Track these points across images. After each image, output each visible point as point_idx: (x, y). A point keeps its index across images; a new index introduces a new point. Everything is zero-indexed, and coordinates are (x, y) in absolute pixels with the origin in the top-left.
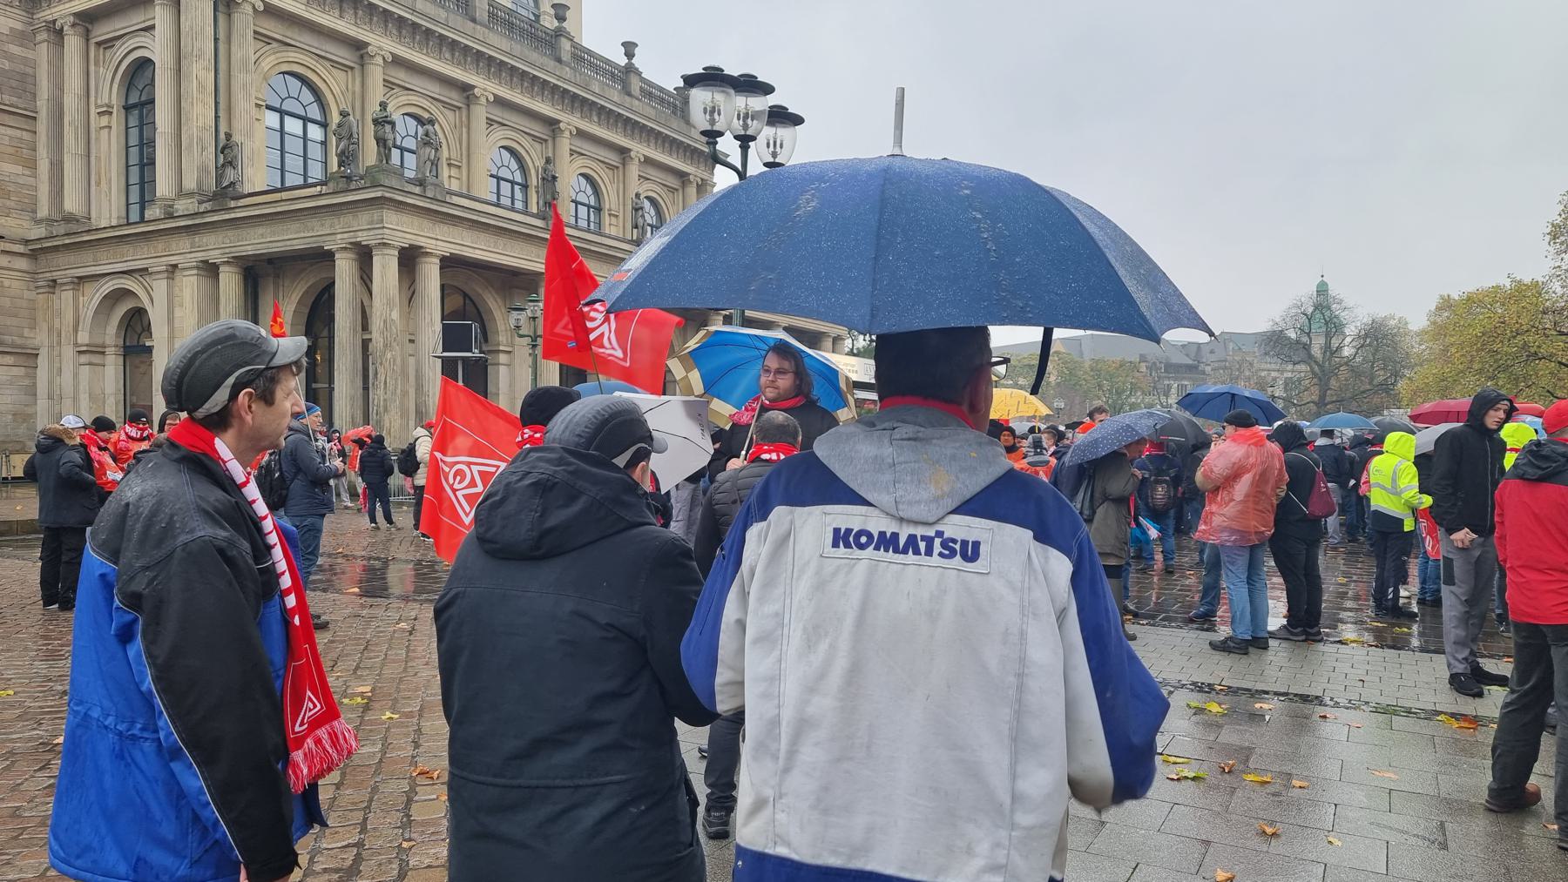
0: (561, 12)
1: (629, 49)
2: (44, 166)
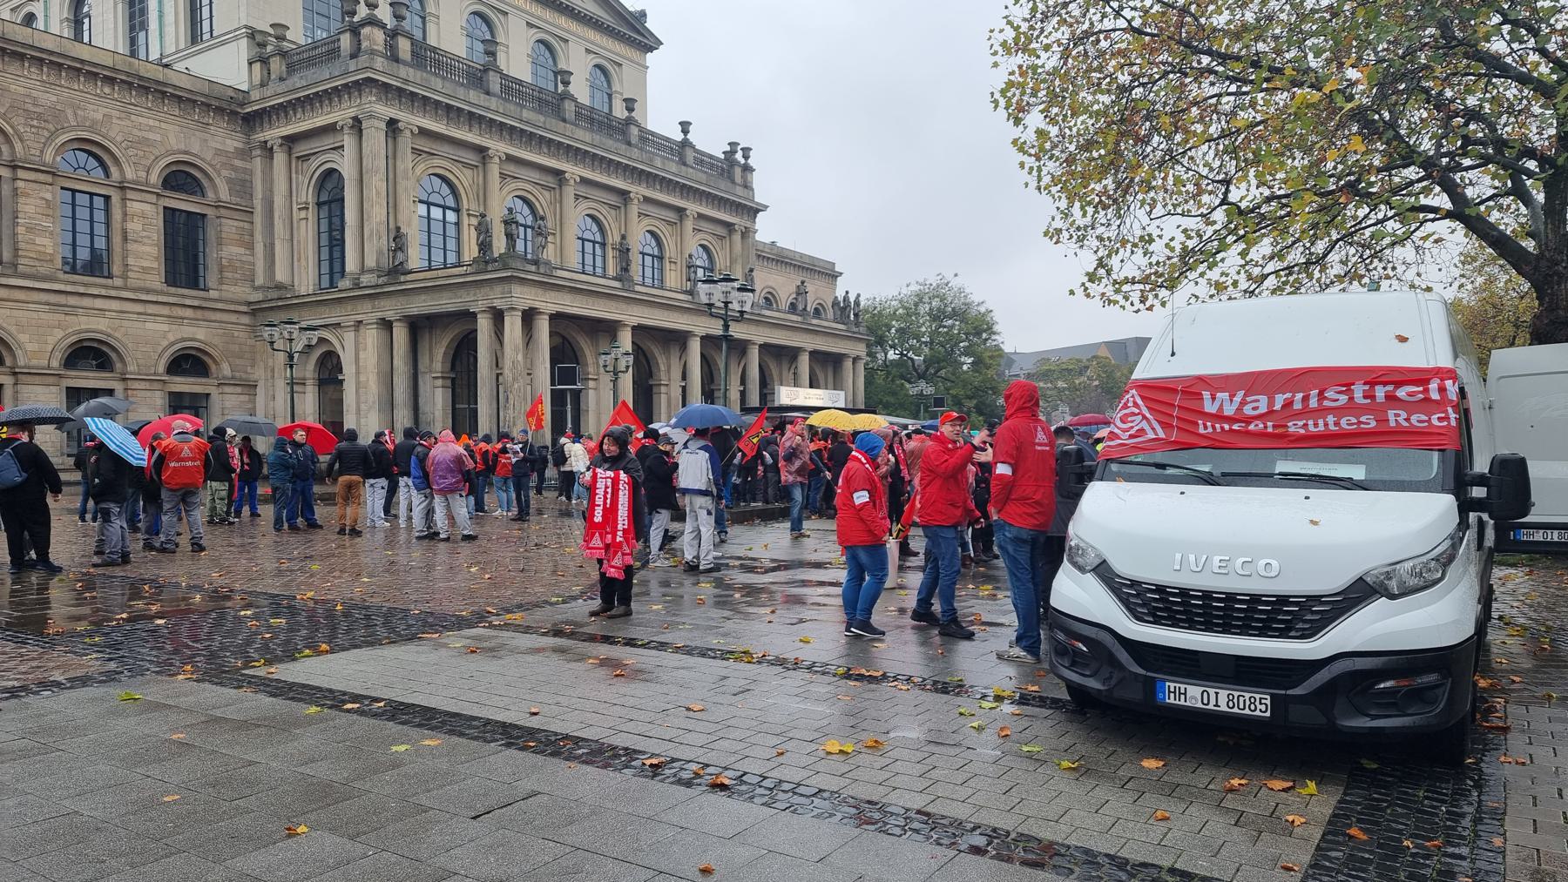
0: (630, 105)
1: (685, 127)
2: (259, 248)
